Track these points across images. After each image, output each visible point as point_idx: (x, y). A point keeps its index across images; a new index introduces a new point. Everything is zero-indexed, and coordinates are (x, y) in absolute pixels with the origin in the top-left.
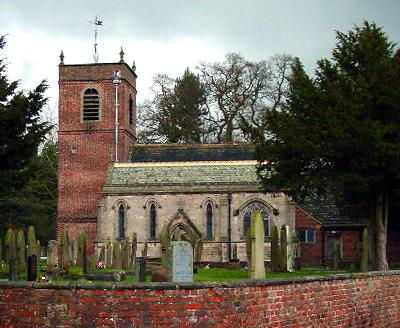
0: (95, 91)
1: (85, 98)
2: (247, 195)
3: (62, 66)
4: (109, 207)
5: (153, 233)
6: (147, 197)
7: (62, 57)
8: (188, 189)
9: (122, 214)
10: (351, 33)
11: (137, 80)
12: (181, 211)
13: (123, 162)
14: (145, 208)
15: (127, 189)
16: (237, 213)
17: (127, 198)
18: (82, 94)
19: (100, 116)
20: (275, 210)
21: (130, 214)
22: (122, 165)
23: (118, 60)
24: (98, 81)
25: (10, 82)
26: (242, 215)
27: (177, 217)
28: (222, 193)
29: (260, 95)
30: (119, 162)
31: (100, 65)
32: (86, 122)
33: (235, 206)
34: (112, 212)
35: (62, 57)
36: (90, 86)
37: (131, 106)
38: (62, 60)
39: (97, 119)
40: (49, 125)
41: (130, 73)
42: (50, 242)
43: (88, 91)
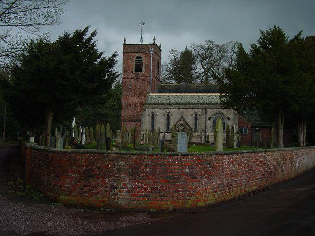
0: (140, 58)
4: (147, 114)
5: (168, 128)
7: (125, 40)
16: (210, 119)
17: (156, 111)
18: (134, 59)
19: (143, 70)
21: (157, 118)
33: (208, 115)
34: (148, 117)
35: (125, 40)
37: (158, 65)
43: (137, 58)
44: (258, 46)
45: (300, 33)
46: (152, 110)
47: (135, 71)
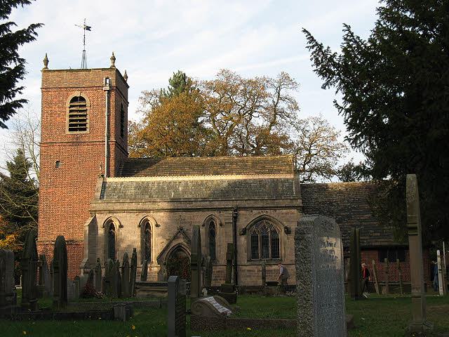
0: (82, 99)
1: (71, 106)
2: (255, 211)
3: (46, 71)
6: (141, 216)
7: (46, 62)
8: (188, 206)
10: (334, 56)
11: (129, 90)
12: (181, 229)
15: (194, 205)
16: (244, 232)
20: (286, 228)
23: (108, 65)
24: (86, 88)
26: (249, 234)
27: (175, 237)
28: (226, 209)
29: (254, 114)
30: (117, 175)
31: (87, 70)
32: (71, 133)
35: (46, 62)
36: (77, 94)
38: (47, 65)
39: (85, 129)
40: (130, 255)
41: (120, 86)
43: (75, 99)
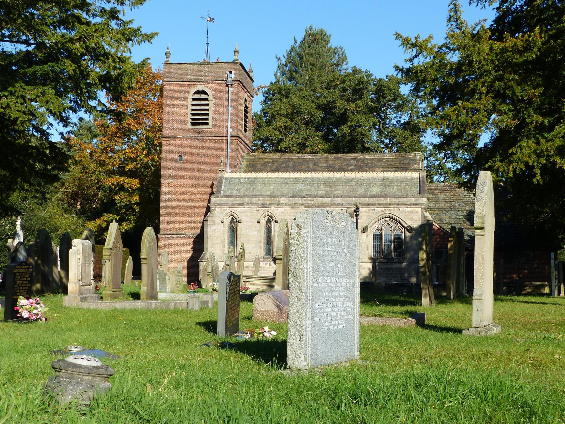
0: (204, 93)
4: (218, 221)
5: (268, 251)
6: (262, 211)
7: (167, 54)
9: (233, 230)
13: (236, 171)
14: (258, 222)
16: (365, 230)
17: (240, 213)
18: (191, 96)
19: (210, 122)
21: (241, 229)
22: (233, 175)
25: (152, 40)
33: (362, 222)
34: (220, 226)
35: (167, 54)
36: (200, 88)
37: (246, 112)
39: (207, 124)
42: (53, 90)
43: (198, 92)
44: (259, 113)
45: (157, 230)
46: (231, 210)
47: (193, 124)
